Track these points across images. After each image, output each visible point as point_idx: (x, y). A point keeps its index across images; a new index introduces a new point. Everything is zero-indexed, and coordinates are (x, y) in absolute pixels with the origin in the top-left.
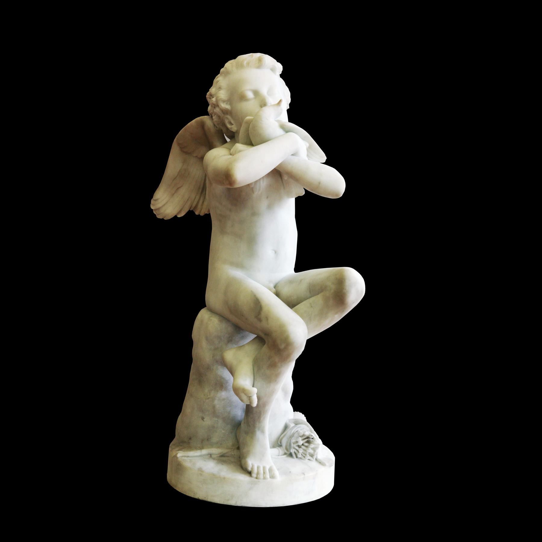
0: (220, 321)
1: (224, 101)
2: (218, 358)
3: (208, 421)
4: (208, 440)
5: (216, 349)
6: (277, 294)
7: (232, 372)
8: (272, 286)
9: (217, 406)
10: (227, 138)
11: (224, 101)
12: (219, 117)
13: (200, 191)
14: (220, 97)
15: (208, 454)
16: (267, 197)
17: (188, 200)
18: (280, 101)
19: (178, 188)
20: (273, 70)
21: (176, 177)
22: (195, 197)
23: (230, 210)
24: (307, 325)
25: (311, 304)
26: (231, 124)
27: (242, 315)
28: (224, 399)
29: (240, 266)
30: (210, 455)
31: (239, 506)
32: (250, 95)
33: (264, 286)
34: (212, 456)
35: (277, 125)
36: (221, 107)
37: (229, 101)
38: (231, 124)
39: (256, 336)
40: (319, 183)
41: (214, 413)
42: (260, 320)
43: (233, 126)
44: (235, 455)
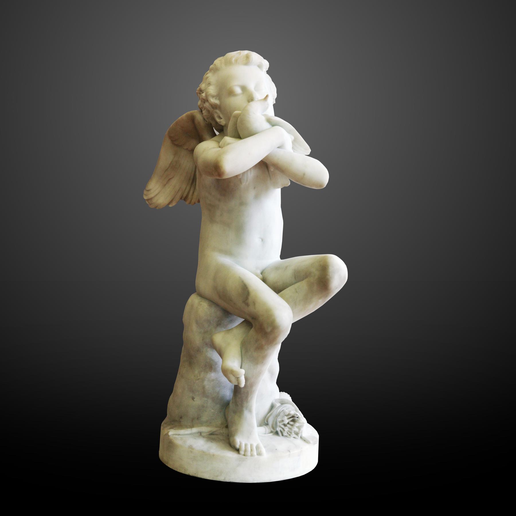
0: (210, 306)
1: (213, 97)
2: (207, 341)
3: (198, 401)
4: (198, 419)
5: (206, 332)
6: (264, 280)
7: (221, 354)
8: (259, 272)
9: (207, 387)
10: (216, 131)
11: (213, 97)
12: (208, 111)
13: (191, 181)
14: (210, 93)
15: (198, 433)
16: (255, 188)
17: (179, 190)
18: (267, 96)
19: (170, 179)
20: (260, 66)
21: (168, 168)
22: (186, 188)
23: (219, 200)
24: (293, 310)
25: (296, 289)
26: (220, 118)
27: (231, 300)
28: (213, 380)
29: (228, 253)
30: (200, 434)
31: (228, 481)
32: (238, 90)
33: (251, 272)
34: (202, 434)
35: (263, 119)
36: (211, 102)
37: (218, 96)
38: (220, 118)
39: (244, 320)
40: (304, 174)
41: (204, 394)
42: (247, 305)
43: (222, 120)
44: (223, 433)
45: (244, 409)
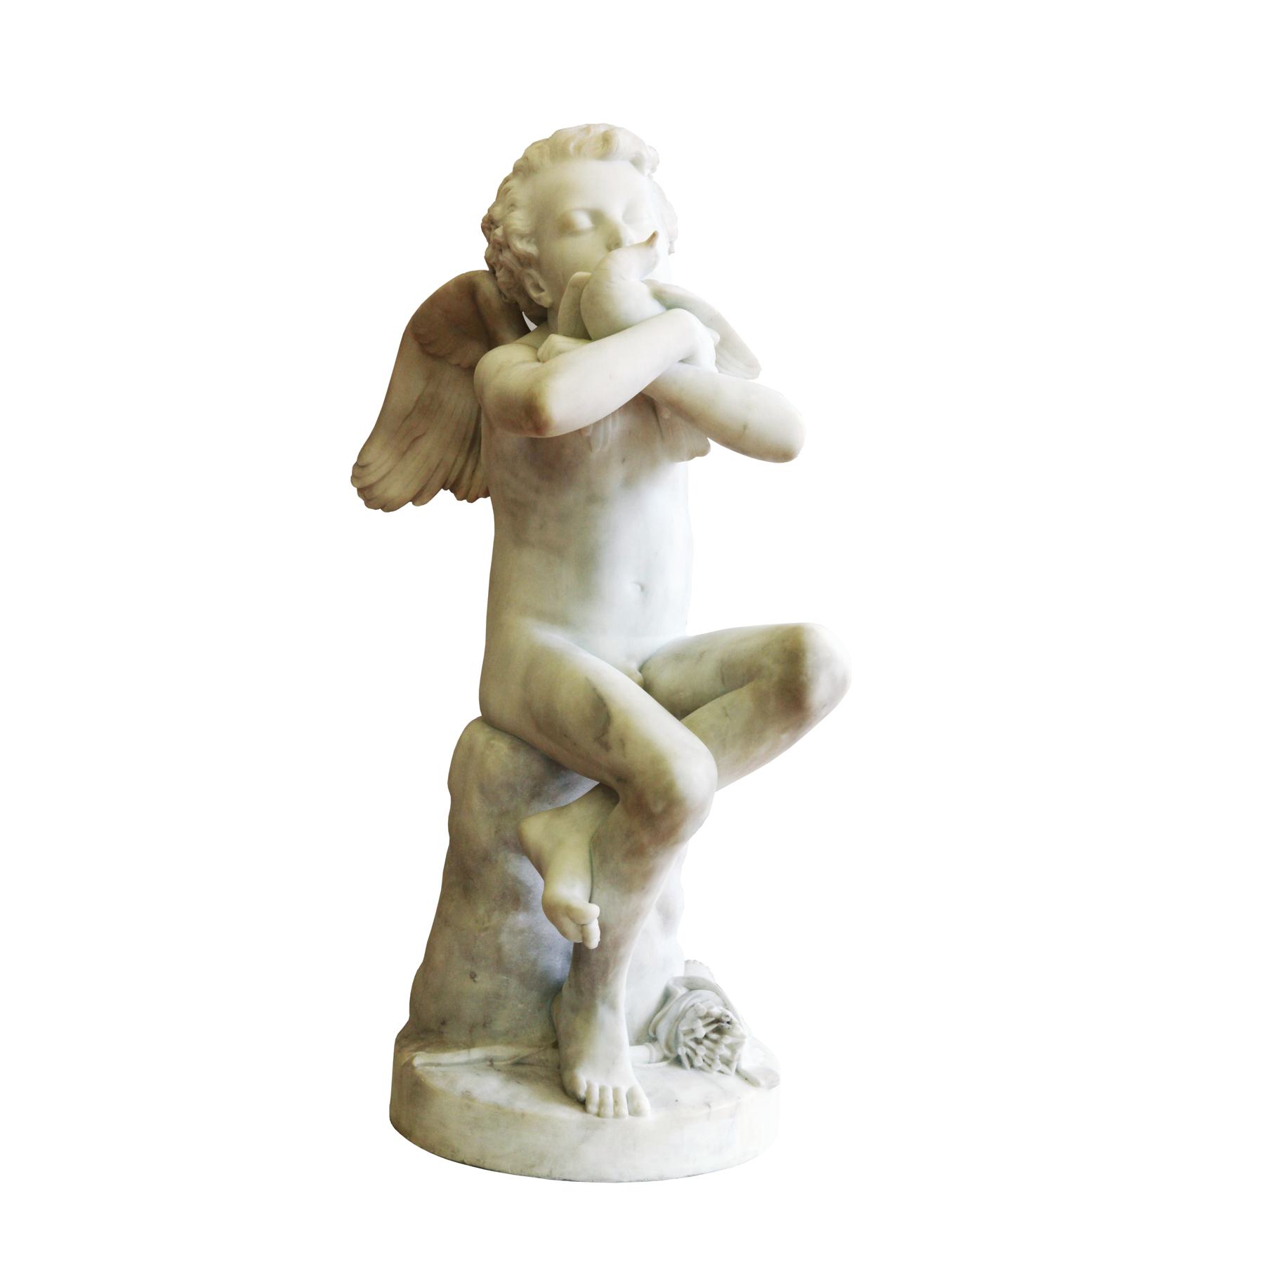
0: (514, 749)
1: (522, 236)
2: (508, 835)
3: (485, 983)
4: (484, 1025)
5: (504, 814)
6: (647, 686)
7: (541, 868)
8: (634, 666)
9: (507, 948)
10: (530, 321)
11: (522, 236)
12: (511, 272)
13: (467, 444)
14: (514, 227)
15: (485, 1060)
16: (624, 460)
17: (438, 466)
18: (654, 235)
19: (415, 439)
21: (411, 413)
22: (456, 460)
23: (537, 491)
24: (717, 759)
25: (724, 708)
26: (539, 288)
27: (565, 736)
28: (522, 932)
29: (559, 619)
30: (491, 1062)
32: (583, 221)
33: (615, 667)
34: (495, 1063)
35: (645, 290)
36: (516, 249)
37: (535, 235)
38: (539, 288)
39: (597, 783)
40: (745, 427)
41: (500, 964)
42: (606, 746)
43: (543, 294)
44: (547, 1061)
45: (598, 1002)
